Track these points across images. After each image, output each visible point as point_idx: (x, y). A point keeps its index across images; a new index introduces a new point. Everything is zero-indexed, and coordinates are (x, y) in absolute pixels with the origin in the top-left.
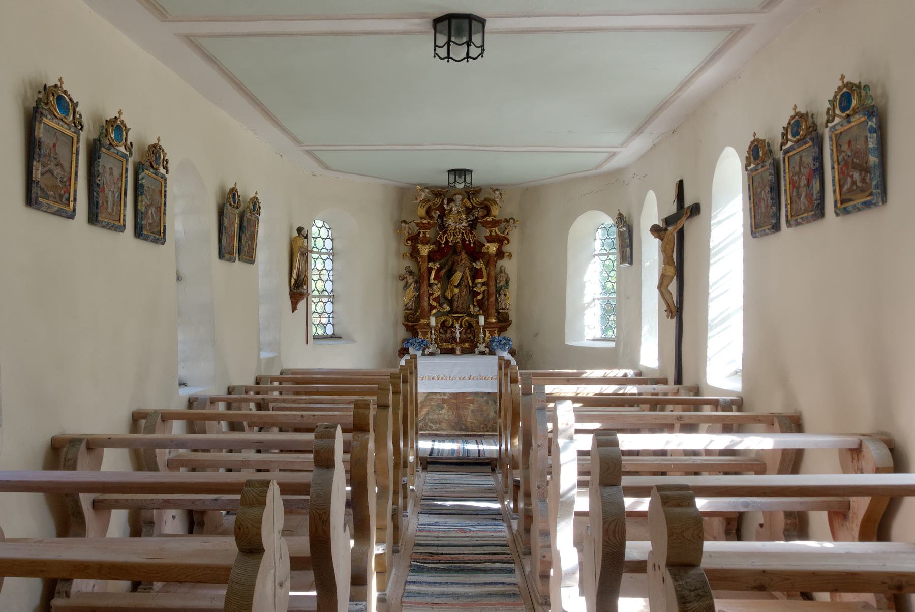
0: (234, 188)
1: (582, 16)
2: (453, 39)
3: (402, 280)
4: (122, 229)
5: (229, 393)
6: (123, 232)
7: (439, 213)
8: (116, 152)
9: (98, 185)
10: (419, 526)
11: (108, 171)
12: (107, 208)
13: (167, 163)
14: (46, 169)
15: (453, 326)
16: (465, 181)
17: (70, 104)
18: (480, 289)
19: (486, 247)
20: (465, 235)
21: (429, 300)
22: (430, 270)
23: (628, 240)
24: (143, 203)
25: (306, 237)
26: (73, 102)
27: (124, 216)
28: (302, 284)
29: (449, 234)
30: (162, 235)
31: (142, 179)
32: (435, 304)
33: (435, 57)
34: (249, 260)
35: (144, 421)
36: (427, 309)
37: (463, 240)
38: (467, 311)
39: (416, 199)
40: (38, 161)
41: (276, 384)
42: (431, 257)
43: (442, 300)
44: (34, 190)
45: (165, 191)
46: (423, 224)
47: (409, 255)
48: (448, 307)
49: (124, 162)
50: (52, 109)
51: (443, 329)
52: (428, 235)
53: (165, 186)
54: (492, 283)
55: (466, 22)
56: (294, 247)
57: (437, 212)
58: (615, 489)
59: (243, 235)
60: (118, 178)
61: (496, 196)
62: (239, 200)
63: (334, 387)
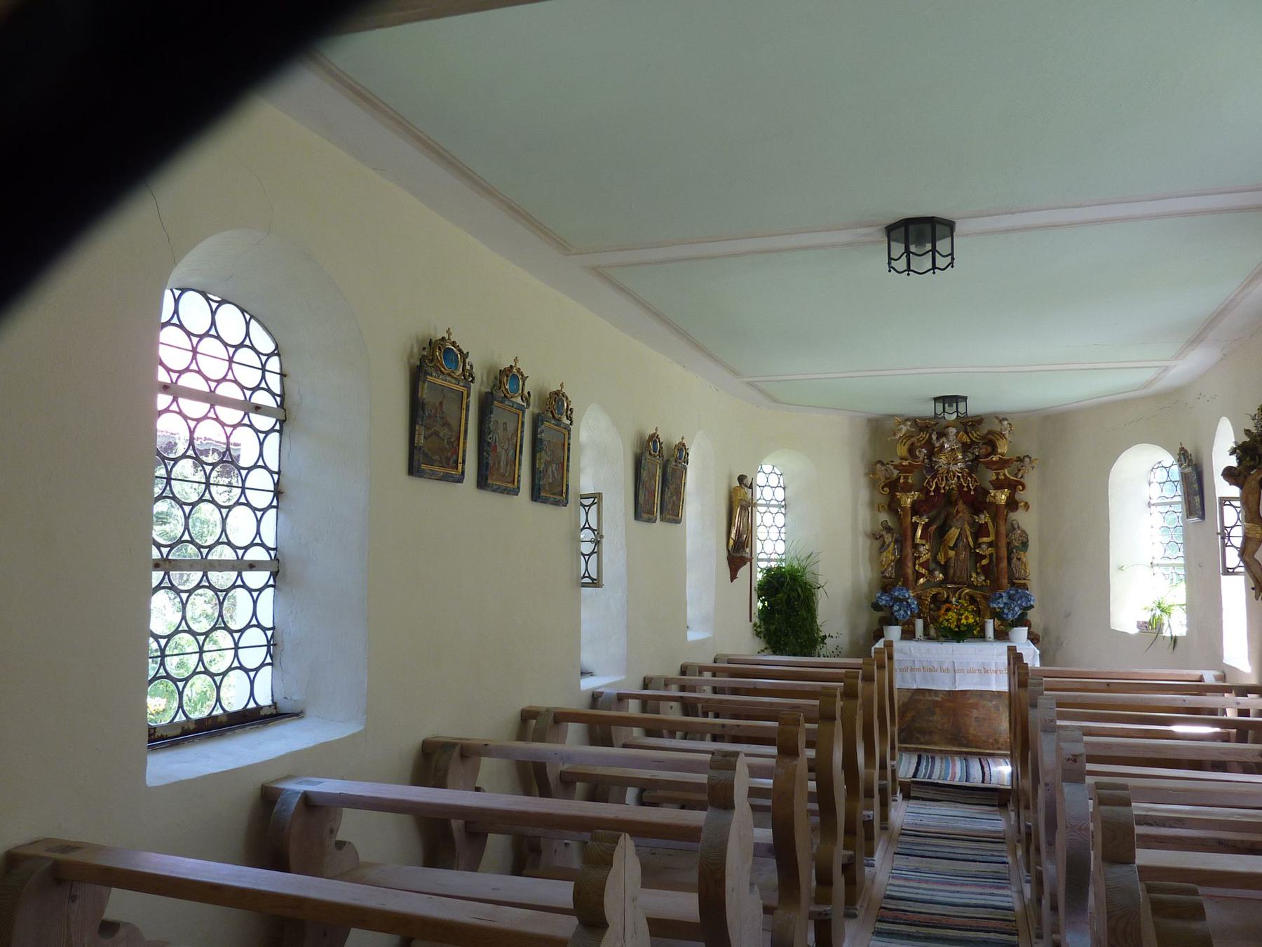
0: (654, 434)
1: (1085, 206)
2: (913, 248)
3: (877, 539)
4: (516, 492)
5: (645, 687)
6: (517, 495)
7: (926, 452)
8: (511, 404)
9: (489, 444)
10: (893, 871)
11: (501, 427)
12: (498, 470)
13: (572, 412)
14: (431, 431)
15: (948, 601)
16: (957, 411)
17: (459, 356)
18: (985, 550)
19: (992, 494)
20: (962, 480)
21: (914, 565)
22: (915, 526)
23: (1196, 486)
24: (542, 460)
25: (751, 487)
26: (463, 352)
27: (519, 476)
28: (744, 546)
29: (940, 478)
30: (564, 495)
31: (541, 432)
32: (923, 571)
33: (890, 271)
34: (674, 520)
35: (534, 721)
36: (911, 578)
37: (960, 487)
38: (967, 580)
39: (895, 435)
40: (422, 425)
41: (707, 675)
42: (916, 509)
43: (932, 566)
44: (416, 457)
45: (569, 444)
46: (903, 466)
47: (886, 507)
48: (941, 575)
49: (521, 415)
50: (439, 365)
51: (934, 604)
52: (910, 481)
53: (569, 438)
54: (1003, 544)
55: (928, 227)
56: (733, 500)
57: (923, 450)
58: (1125, 868)
59: (667, 490)
60: (513, 434)
61: (1003, 427)
62: (661, 447)
63: (779, 683)
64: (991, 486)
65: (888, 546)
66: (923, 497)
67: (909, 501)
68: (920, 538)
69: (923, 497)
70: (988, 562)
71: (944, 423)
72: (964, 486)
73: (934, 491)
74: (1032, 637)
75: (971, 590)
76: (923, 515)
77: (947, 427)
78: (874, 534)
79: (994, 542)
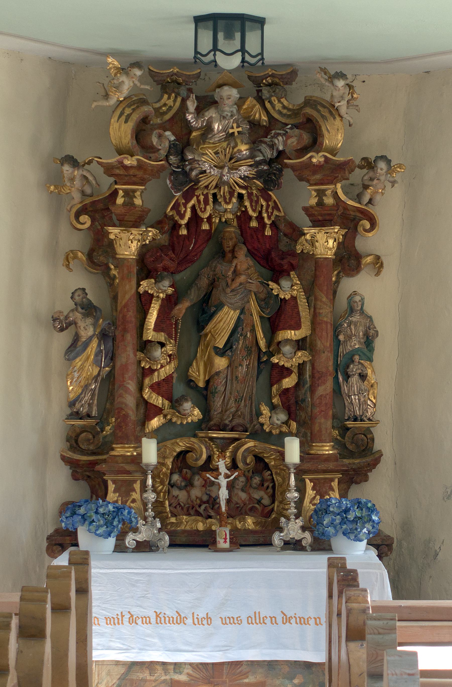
16: (243, 50)
19: (308, 237)
20: (247, 203)
21: (141, 389)
29: (202, 198)
38: (251, 421)
39: (106, 96)
46: (126, 168)
48: (197, 412)
51: (180, 472)
55: (238, 24)
57: (168, 133)
61: (335, 93)
64: (307, 219)
65: (86, 344)
66: (163, 239)
67: (134, 246)
68: (155, 330)
69: (163, 239)
70: (293, 383)
71: (216, 78)
72: (250, 218)
73: (188, 225)
74: (379, 542)
75: (257, 443)
76: (162, 279)
77: (220, 86)
78: (54, 320)
79: (308, 339)
